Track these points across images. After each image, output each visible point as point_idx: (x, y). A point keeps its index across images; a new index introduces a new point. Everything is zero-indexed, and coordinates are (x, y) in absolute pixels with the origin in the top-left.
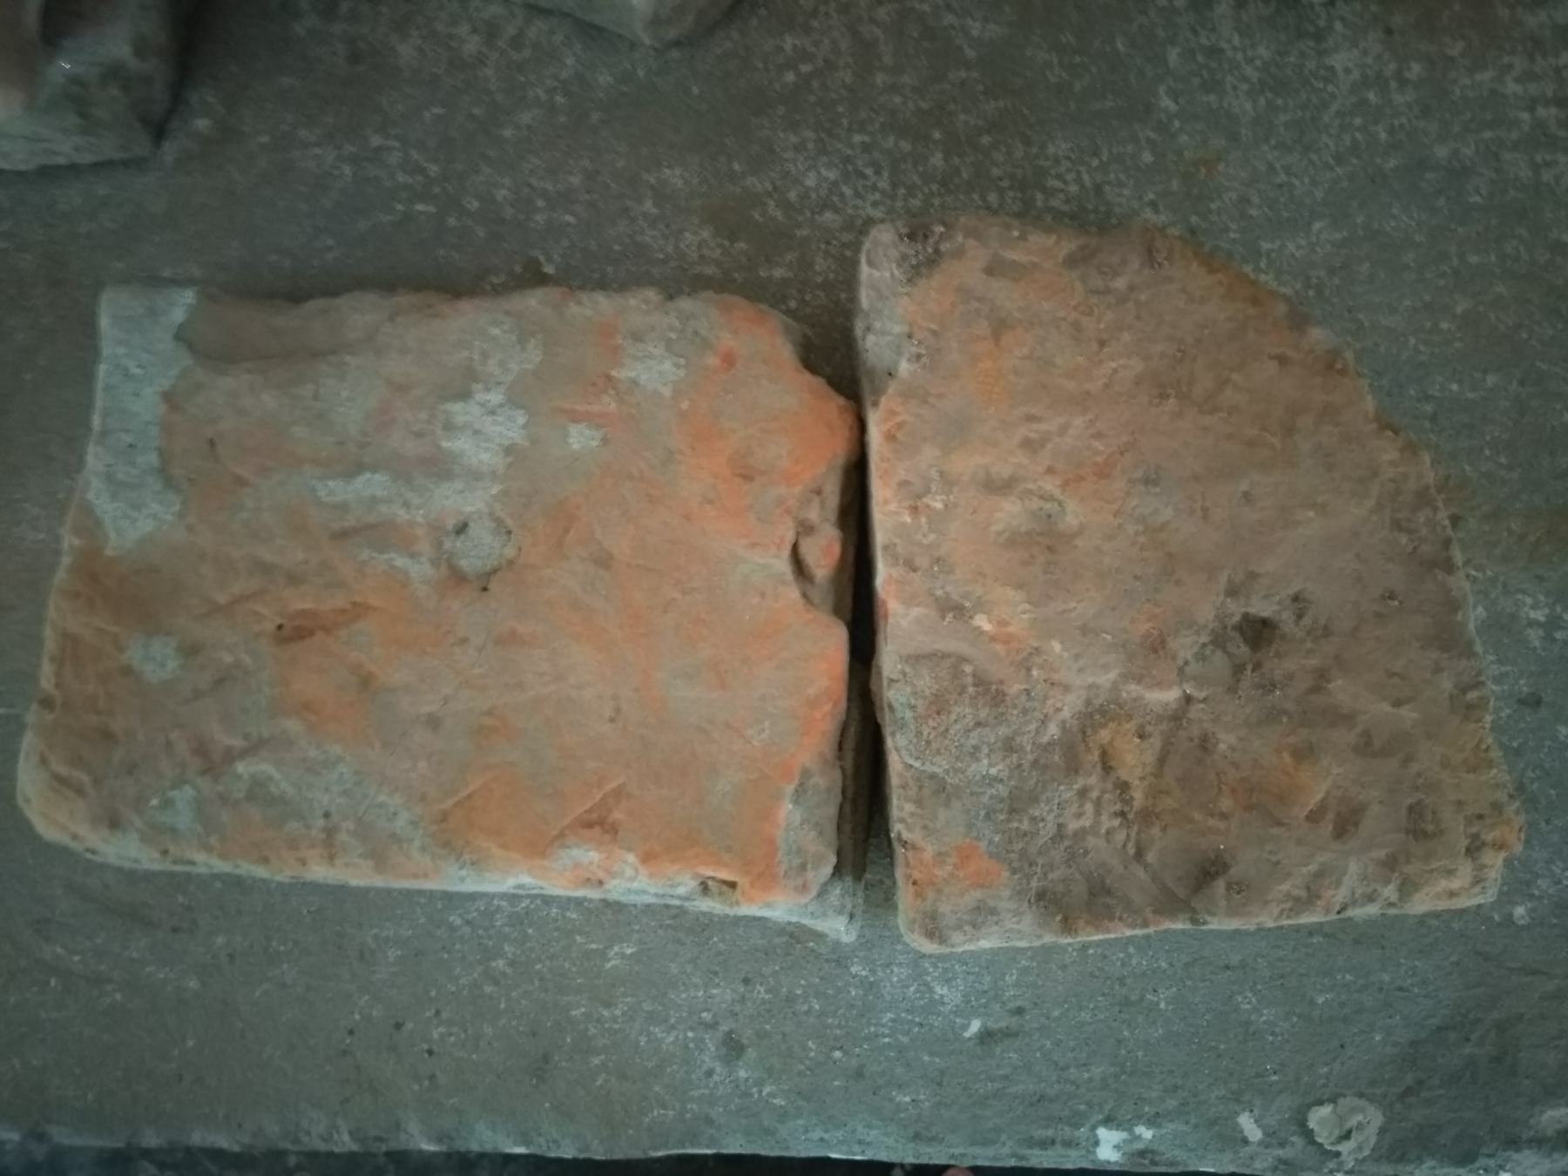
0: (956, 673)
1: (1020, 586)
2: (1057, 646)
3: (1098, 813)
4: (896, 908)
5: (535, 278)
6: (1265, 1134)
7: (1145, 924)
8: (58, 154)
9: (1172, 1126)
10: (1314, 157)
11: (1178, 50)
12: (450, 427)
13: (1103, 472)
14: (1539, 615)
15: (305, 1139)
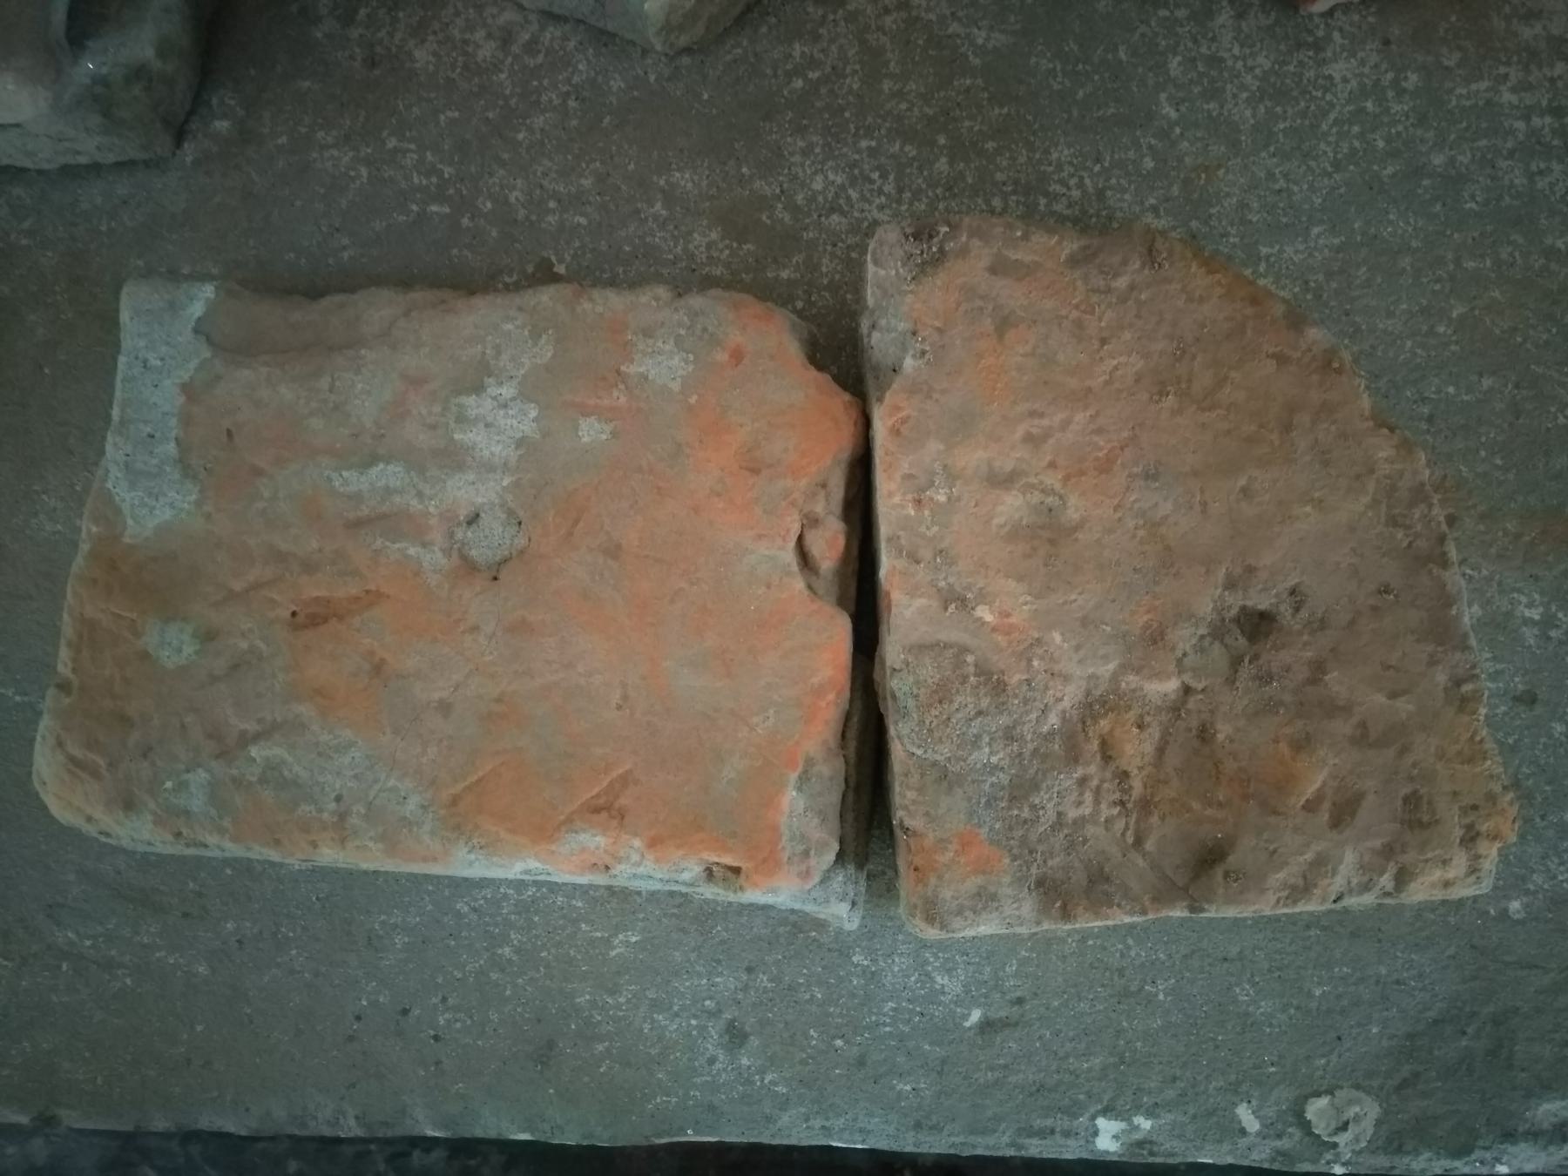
0: (959, 663)
1: (1020, 579)
2: (1057, 637)
3: (1097, 802)
4: (898, 897)
5: (545, 275)
6: (1263, 1125)
7: (1144, 912)
8: (78, 153)
9: (1170, 1117)
10: (1313, 164)
11: (1179, 58)
12: (461, 419)
13: (1105, 467)
14: (1535, 614)
15: (312, 1124)
